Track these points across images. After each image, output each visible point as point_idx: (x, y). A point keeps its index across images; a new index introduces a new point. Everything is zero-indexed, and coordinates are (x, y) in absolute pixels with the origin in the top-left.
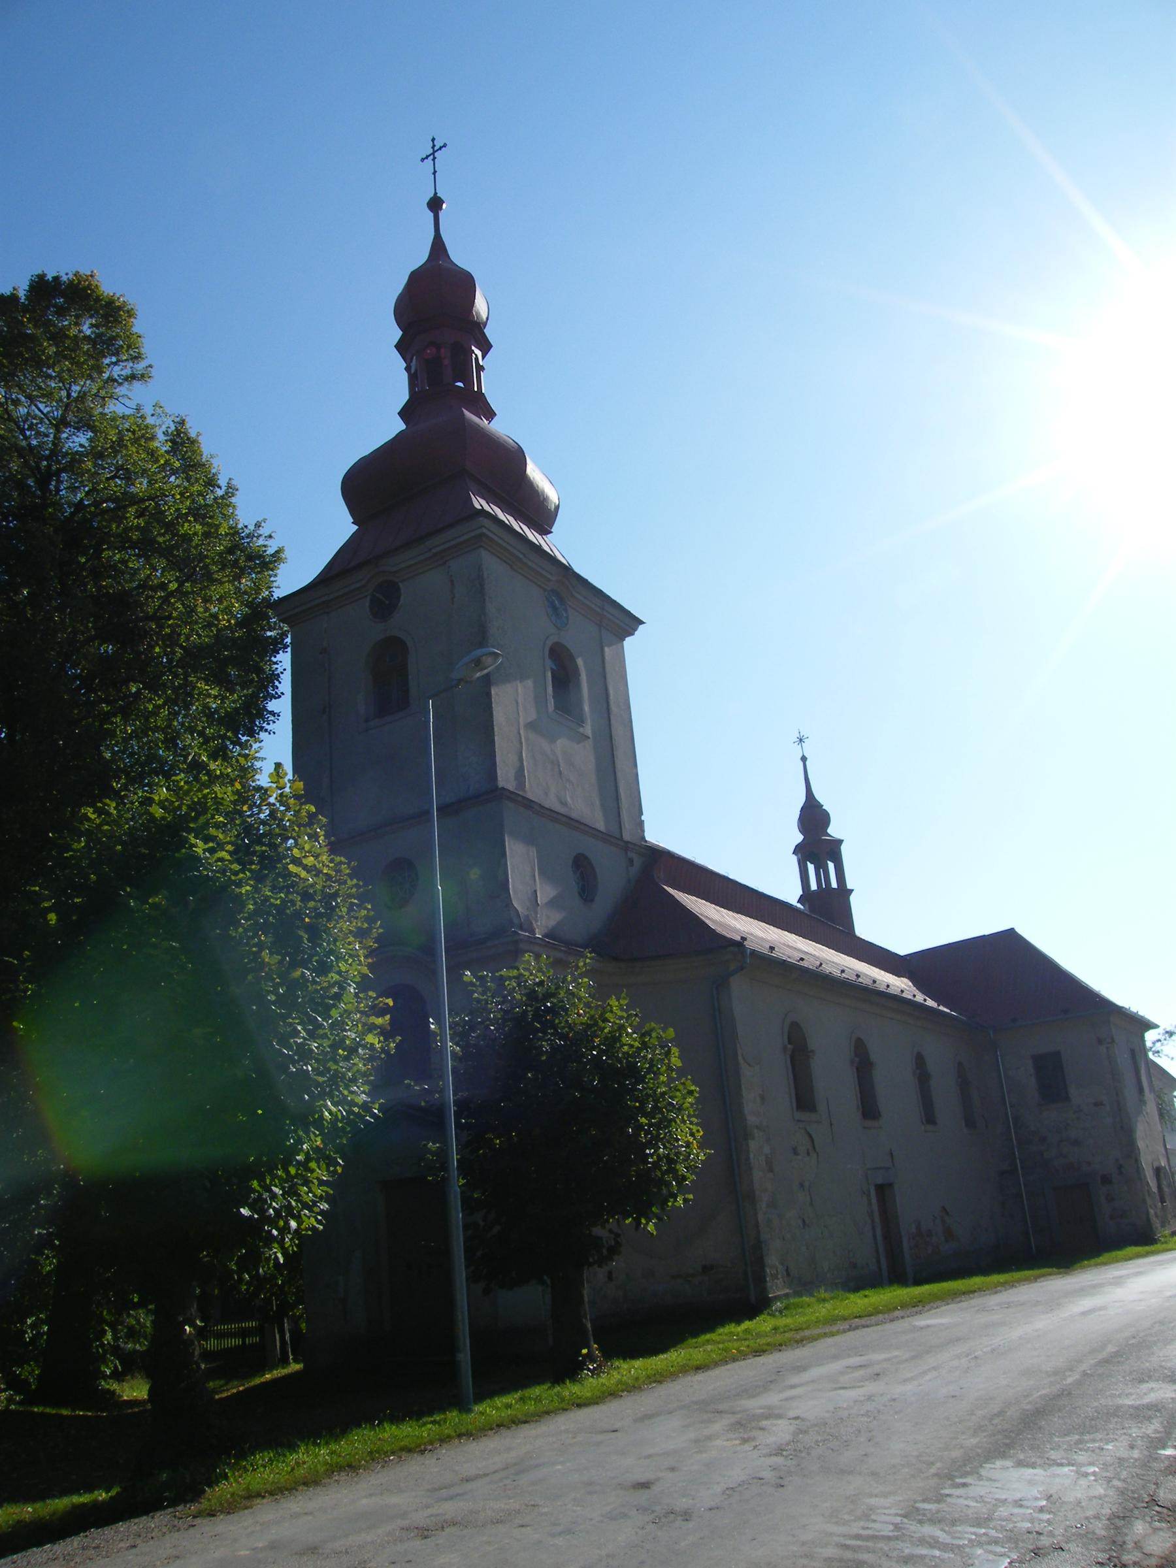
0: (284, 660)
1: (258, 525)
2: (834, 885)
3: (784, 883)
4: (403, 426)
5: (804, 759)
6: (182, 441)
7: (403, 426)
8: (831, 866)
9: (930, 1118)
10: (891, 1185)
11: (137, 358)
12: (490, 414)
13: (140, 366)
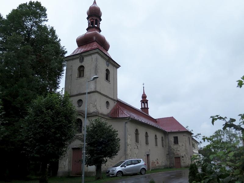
0: (65, 68)
1: (64, 47)
2: (146, 107)
3: (138, 106)
4: (5, 17)
5: (144, 87)
6: (53, 31)
7: (5, 17)
8: (146, 104)
9: (156, 145)
10: (149, 155)
11: (46, 17)
12: (100, 31)
13: (46, 19)
